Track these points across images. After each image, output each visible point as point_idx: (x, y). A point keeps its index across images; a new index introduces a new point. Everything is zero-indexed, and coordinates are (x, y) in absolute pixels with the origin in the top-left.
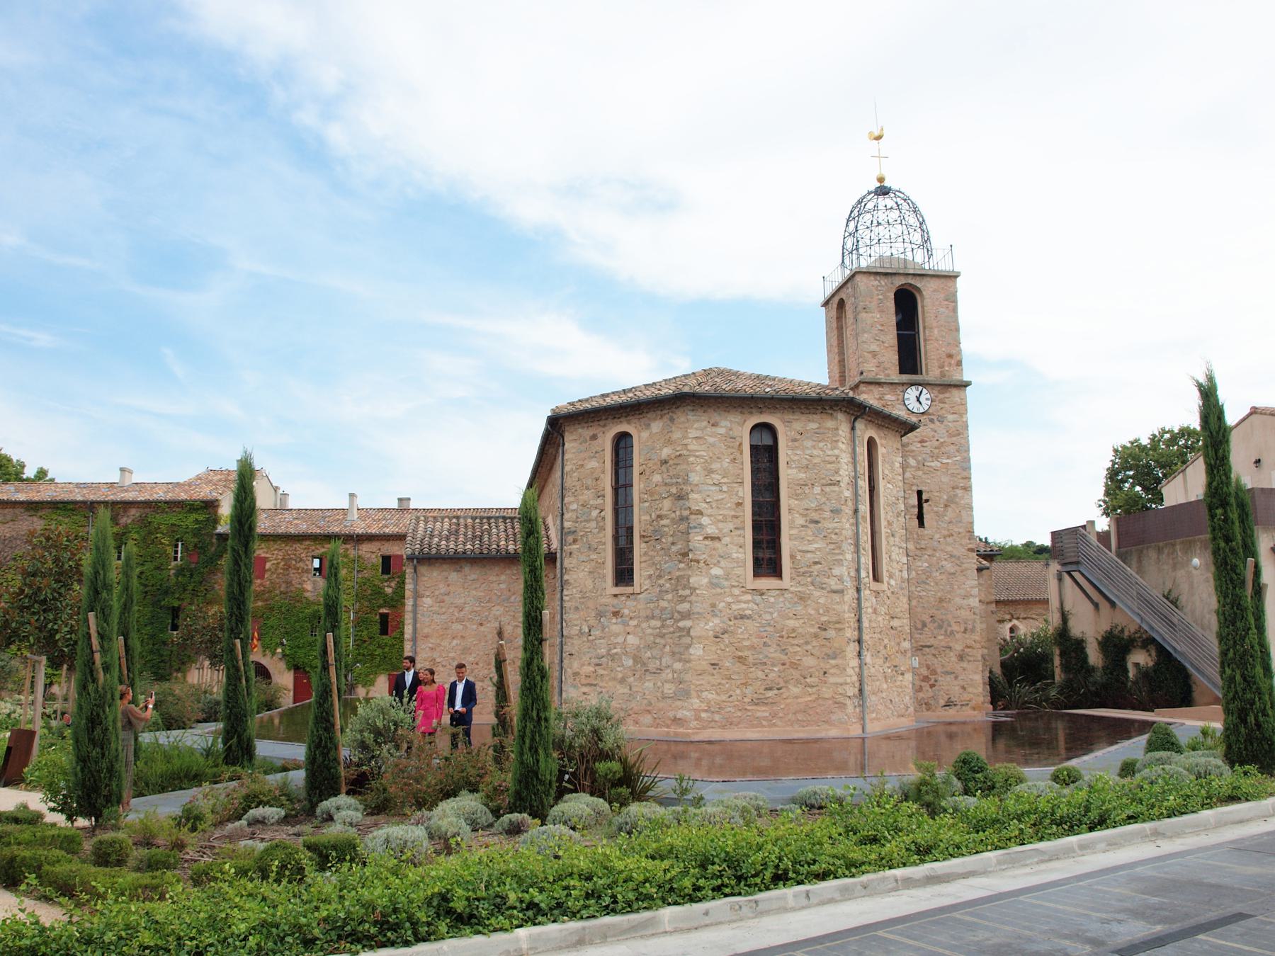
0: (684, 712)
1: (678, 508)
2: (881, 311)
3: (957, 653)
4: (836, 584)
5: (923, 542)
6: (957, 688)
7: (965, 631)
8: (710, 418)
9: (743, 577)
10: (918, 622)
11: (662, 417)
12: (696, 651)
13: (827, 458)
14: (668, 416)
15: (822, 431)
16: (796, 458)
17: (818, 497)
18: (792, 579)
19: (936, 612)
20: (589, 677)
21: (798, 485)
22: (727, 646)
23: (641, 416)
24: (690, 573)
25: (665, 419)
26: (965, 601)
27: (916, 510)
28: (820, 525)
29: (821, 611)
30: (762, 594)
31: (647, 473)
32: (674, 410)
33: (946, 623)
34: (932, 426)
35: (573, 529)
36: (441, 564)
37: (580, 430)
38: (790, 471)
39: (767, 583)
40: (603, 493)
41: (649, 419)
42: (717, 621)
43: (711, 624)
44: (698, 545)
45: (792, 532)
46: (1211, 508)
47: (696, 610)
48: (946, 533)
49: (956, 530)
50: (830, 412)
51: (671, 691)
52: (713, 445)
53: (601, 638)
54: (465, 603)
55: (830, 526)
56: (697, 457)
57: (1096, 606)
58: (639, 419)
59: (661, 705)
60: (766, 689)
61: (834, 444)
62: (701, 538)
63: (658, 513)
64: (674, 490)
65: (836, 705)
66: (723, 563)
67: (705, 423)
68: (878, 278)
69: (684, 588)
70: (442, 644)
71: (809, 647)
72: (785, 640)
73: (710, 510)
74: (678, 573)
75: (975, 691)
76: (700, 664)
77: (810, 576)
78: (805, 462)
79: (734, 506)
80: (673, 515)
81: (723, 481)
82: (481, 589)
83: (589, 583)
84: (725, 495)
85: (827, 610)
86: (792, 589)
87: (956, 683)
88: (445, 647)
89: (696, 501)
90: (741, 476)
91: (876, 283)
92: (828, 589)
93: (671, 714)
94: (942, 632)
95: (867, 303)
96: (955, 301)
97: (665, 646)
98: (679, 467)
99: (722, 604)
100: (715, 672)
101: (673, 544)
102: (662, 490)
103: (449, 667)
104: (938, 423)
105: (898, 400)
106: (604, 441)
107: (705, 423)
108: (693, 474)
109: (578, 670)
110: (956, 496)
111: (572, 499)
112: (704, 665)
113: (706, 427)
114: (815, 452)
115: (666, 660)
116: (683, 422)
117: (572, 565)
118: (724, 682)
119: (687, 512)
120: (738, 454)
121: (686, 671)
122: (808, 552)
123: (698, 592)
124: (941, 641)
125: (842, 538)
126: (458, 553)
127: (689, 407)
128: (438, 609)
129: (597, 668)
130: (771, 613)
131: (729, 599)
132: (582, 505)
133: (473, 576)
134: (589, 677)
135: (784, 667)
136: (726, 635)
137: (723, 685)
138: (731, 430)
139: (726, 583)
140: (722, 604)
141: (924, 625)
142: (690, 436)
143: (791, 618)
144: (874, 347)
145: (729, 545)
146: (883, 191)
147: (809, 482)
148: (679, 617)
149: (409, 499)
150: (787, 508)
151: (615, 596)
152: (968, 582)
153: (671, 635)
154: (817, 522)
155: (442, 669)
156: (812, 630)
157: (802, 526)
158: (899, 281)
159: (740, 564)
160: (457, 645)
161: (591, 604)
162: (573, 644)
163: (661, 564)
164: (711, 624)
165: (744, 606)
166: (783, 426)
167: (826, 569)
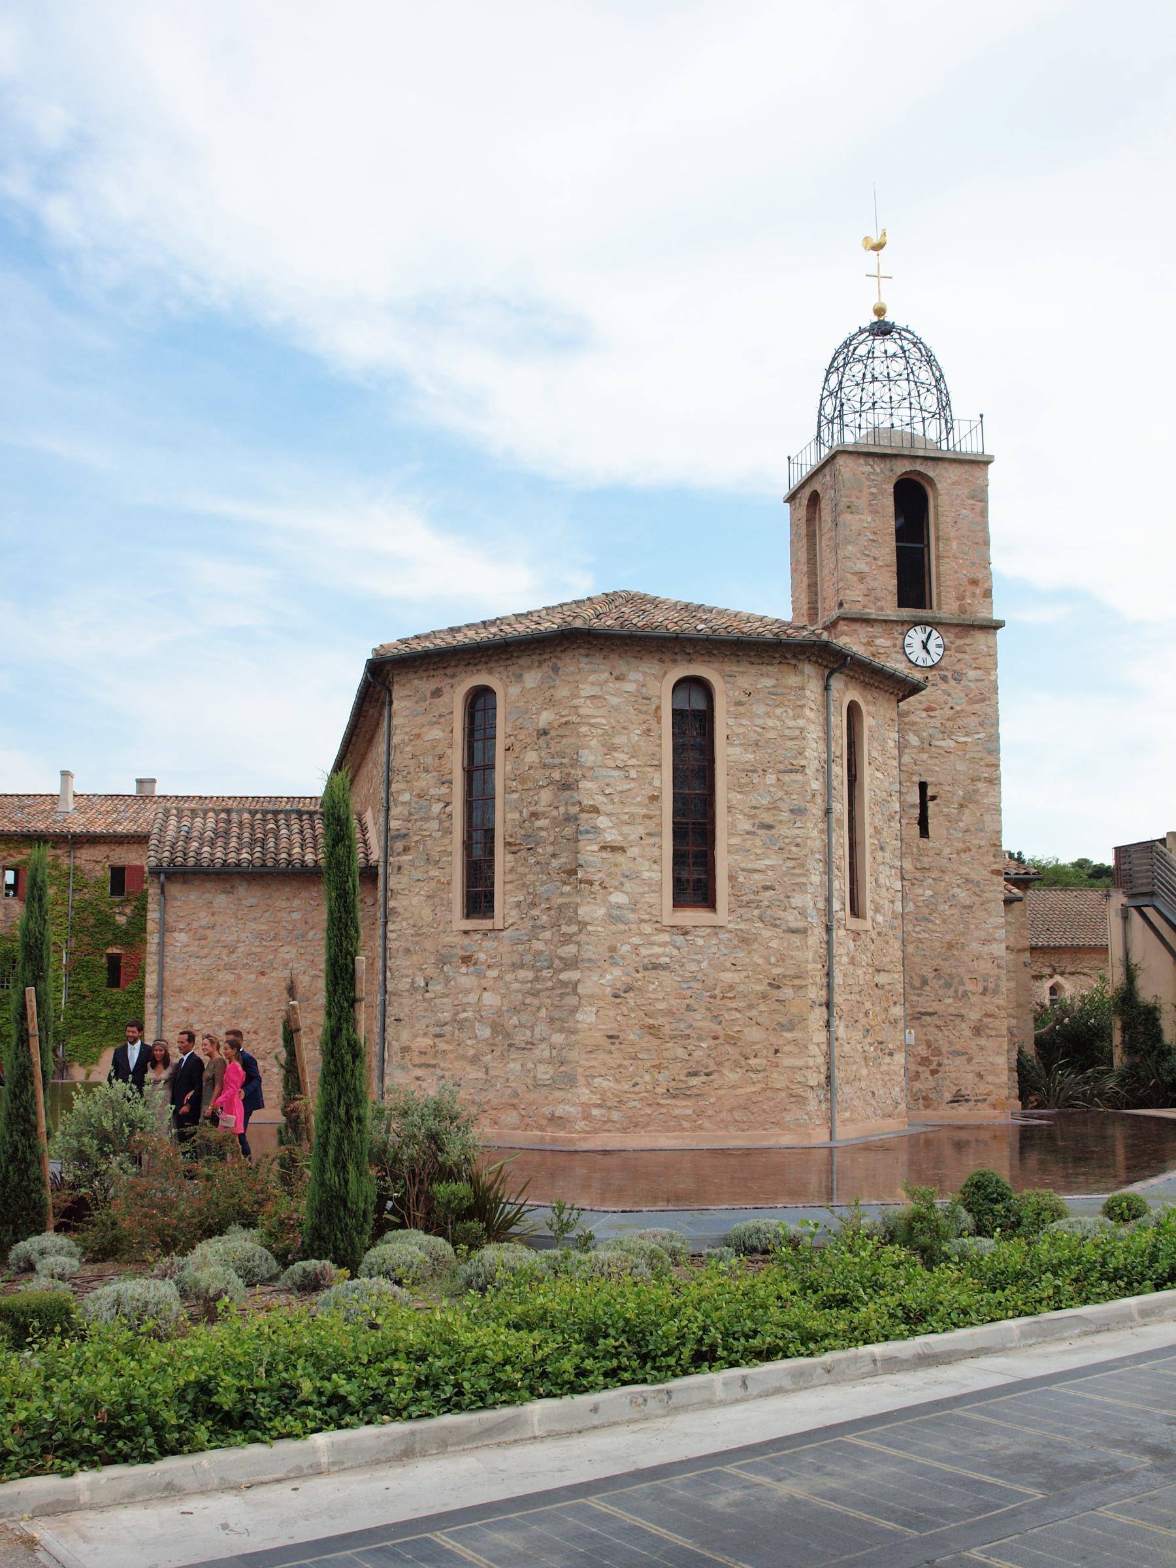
0: (567, 1108)
1: (563, 803)
2: (875, 512)
3: (972, 1024)
4: (796, 919)
5: (926, 859)
6: (970, 1076)
7: (984, 992)
10: (915, 977)
11: (540, 665)
12: (586, 1017)
13: (787, 732)
14: (550, 664)
15: (779, 690)
16: (741, 730)
17: (772, 789)
18: (731, 911)
19: (942, 963)
20: (425, 1053)
21: (743, 771)
22: (632, 1010)
23: (509, 662)
24: (578, 900)
26: (986, 948)
27: (917, 812)
28: (774, 831)
29: (773, 960)
30: (686, 933)
33: (956, 980)
34: (944, 686)
35: (404, 831)
37: (416, 682)
38: (731, 750)
40: (449, 777)
41: (521, 667)
42: (617, 972)
43: (608, 977)
44: (591, 858)
45: (735, 841)
47: (587, 955)
48: (960, 846)
49: (975, 842)
50: (793, 662)
51: (548, 1077)
52: (617, 708)
54: (238, 941)
55: (789, 833)
56: (592, 725)
58: (506, 666)
59: (531, 1096)
60: (689, 1074)
61: (798, 710)
62: (595, 848)
63: (532, 809)
64: (556, 775)
65: (793, 1100)
66: (628, 886)
67: (605, 675)
68: (871, 461)
70: (204, 1002)
71: (754, 1013)
72: (718, 1001)
74: (560, 901)
75: (997, 1081)
76: (591, 1036)
77: (756, 908)
78: (755, 737)
80: (555, 813)
81: (630, 763)
83: (427, 914)
84: (632, 785)
85: (782, 959)
86: (731, 926)
88: (207, 1007)
90: (658, 757)
92: (784, 927)
93: (547, 1110)
94: (951, 992)
95: (853, 499)
96: (984, 500)
97: (539, 1008)
98: (564, 740)
99: (626, 948)
100: (613, 1048)
101: (554, 856)
104: (953, 683)
105: (895, 646)
107: (605, 675)
108: (586, 752)
109: (408, 1043)
110: (976, 791)
113: (606, 681)
114: (770, 723)
116: (572, 673)
117: (401, 886)
119: (576, 809)
121: (570, 1046)
122: (756, 871)
124: (949, 1005)
125: (806, 851)
126: (229, 865)
129: (437, 1040)
130: (699, 962)
131: (636, 940)
133: (251, 901)
134: (425, 1053)
135: (716, 1042)
136: (631, 994)
137: (626, 1067)
139: (632, 917)
140: (626, 948)
141: (925, 982)
142: (583, 693)
143: (728, 970)
144: (862, 566)
145: (639, 860)
146: (882, 329)
147: (760, 768)
149: (153, 781)
151: (466, 932)
152: (991, 920)
153: (548, 993)
156: (759, 988)
157: (748, 833)
158: (902, 467)
160: (225, 1003)
162: (401, 1004)
163: (535, 886)
167: (782, 897)
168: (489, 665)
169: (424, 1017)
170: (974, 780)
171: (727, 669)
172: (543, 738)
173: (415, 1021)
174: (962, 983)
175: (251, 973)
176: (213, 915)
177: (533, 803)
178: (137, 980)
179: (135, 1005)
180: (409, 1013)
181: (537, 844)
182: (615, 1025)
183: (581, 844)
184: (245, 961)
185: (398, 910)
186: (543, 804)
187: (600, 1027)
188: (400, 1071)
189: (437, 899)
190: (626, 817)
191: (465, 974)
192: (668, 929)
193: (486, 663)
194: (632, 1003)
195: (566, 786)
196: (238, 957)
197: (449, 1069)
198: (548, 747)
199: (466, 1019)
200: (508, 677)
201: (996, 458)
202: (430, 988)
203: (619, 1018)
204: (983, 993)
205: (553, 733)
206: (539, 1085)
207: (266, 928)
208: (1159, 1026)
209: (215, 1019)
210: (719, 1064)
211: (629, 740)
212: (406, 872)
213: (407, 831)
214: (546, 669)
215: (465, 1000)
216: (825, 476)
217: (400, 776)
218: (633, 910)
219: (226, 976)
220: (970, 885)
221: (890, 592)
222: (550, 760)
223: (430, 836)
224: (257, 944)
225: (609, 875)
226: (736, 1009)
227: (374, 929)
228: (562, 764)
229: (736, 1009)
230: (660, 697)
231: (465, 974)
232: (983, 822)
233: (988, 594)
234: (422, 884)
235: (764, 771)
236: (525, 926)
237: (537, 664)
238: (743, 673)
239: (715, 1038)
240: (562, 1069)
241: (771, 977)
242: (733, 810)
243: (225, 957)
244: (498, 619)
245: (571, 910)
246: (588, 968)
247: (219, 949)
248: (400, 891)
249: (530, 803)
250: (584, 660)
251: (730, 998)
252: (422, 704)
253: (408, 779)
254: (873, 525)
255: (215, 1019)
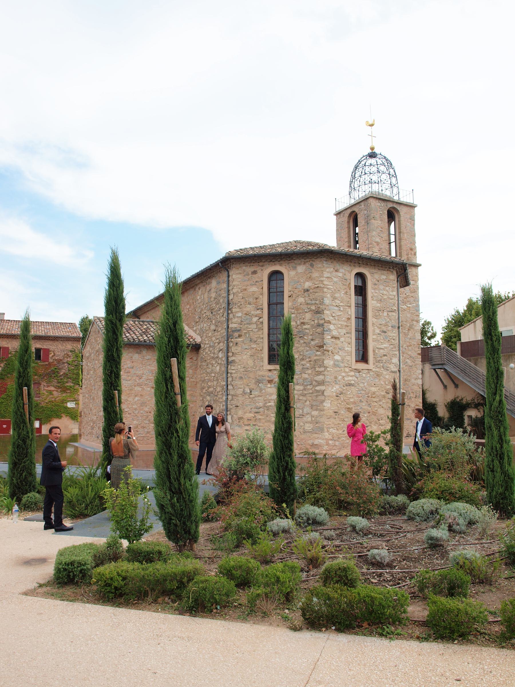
0: (320, 441)
1: (316, 319)
2: (381, 220)
6: (412, 427)
8: (335, 266)
9: (350, 361)
11: (305, 263)
12: (327, 404)
13: (390, 297)
14: (310, 263)
15: (387, 281)
16: (376, 295)
17: (386, 318)
20: (250, 420)
21: (377, 310)
22: (342, 402)
23: (289, 262)
24: (324, 358)
25: (308, 265)
26: (416, 381)
28: (386, 334)
29: (387, 383)
30: (359, 372)
31: (294, 297)
32: (313, 259)
35: (239, 329)
36: (129, 348)
37: (244, 268)
38: (373, 302)
39: (361, 366)
40: (261, 307)
41: (296, 264)
42: (337, 387)
45: (375, 337)
46: (487, 342)
47: (327, 380)
48: (408, 344)
49: (413, 343)
50: (392, 270)
51: (310, 428)
52: (336, 283)
53: (259, 396)
54: (143, 374)
55: (391, 335)
57: (445, 387)
58: (289, 263)
59: (303, 436)
62: (330, 337)
63: (302, 321)
64: (313, 308)
66: (340, 353)
68: (380, 202)
69: (320, 367)
70: (129, 399)
71: (381, 403)
72: (370, 399)
73: (335, 321)
74: (316, 358)
76: (329, 412)
77: (382, 363)
78: (380, 298)
79: (346, 320)
80: (313, 323)
82: (153, 365)
83: (250, 363)
84: (342, 313)
86: (374, 370)
87: (412, 424)
88: (130, 401)
89: (327, 314)
90: (350, 303)
91: (379, 204)
92: (390, 370)
93: (310, 442)
95: (375, 215)
96: (414, 220)
97: (306, 401)
98: (317, 294)
100: (336, 417)
101: (312, 340)
102: (305, 307)
103: (132, 414)
106: (262, 275)
107: (332, 269)
108: (326, 299)
109: (241, 416)
110: (413, 325)
111: (238, 310)
112: (331, 413)
113: (333, 272)
115: (307, 410)
116: (320, 267)
117: (238, 351)
118: (340, 422)
119: (323, 321)
120: (348, 291)
121: (321, 416)
123: (328, 369)
126: (141, 341)
127: (324, 259)
128: (126, 377)
129: (256, 414)
130: (364, 383)
131: (343, 374)
132: (246, 314)
133: (148, 357)
134: (250, 420)
135: (369, 414)
136: (342, 395)
137: (340, 424)
138: (345, 274)
139: (342, 365)
142: (325, 276)
143: (373, 386)
144: (378, 240)
145: (344, 343)
146: (372, 155)
148: (316, 384)
149: (4, 314)
150: (372, 323)
151: (270, 370)
153: (310, 395)
154: (385, 332)
155: (128, 416)
157: (379, 334)
158: (390, 205)
159: (349, 354)
160: (138, 400)
161: (252, 375)
162: (238, 400)
163: (303, 352)
164: (334, 389)
165: (350, 378)
166: (369, 275)
167: (389, 359)
168: (280, 262)
169: (249, 405)
170: (412, 320)
171: (371, 271)
172: (307, 292)
173: (245, 406)
174: (410, 394)
175: (148, 387)
176: (133, 362)
177: (302, 319)
178: (6, 393)
179: (5, 403)
180: (242, 403)
181: (304, 335)
182: (337, 408)
183: (325, 335)
184: (146, 382)
185: (236, 361)
186: (307, 319)
187: (332, 408)
188: (238, 427)
189: (255, 357)
190: (340, 325)
191: (269, 387)
192: (354, 370)
193: (279, 261)
194: (342, 398)
195: (318, 312)
196: (143, 381)
197: (262, 426)
198: (309, 296)
199: (270, 406)
200: (289, 267)
201: (418, 206)
202: (252, 393)
203: (338, 405)
204: (415, 398)
205: (311, 291)
206: (306, 432)
207: (154, 368)
208: (436, 410)
209: (134, 407)
210: (371, 423)
211: (340, 295)
212: (240, 345)
213: (240, 329)
214: (307, 265)
215: (270, 398)
216: (361, 205)
217: (236, 306)
218: (342, 363)
219: (138, 389)
220: (411, 359)
221: (387, 250)
222: (310, 302)
223: (252, 331)
224: (150, 375)
225: (334, 348)
226: (376, 402)
227: (197, 370)
228: (315, 303)
229: (376, 402)
230: (350, 280)
231: (269, 387)
232: (415, 336)
233: (415, 254)
234: (248, 350)
235: (383, 311)
236: (299, 368)
237: (303, 263)
238: (376, 273)
239: (369, 413)
240: (317, 425)
241: (386, 389)
242: (374, 325)
243: (138, 381)
244: (264, 246)
245: (321, 362)
246: (328, 385)
247: (135, 377)
248: (238, 353)
249: (301, 318)
250: (325, 262)
251: (374, 397)
252: (247, 276)
253: (241, 307)
254: (381, 225)
255: (134, 407)
